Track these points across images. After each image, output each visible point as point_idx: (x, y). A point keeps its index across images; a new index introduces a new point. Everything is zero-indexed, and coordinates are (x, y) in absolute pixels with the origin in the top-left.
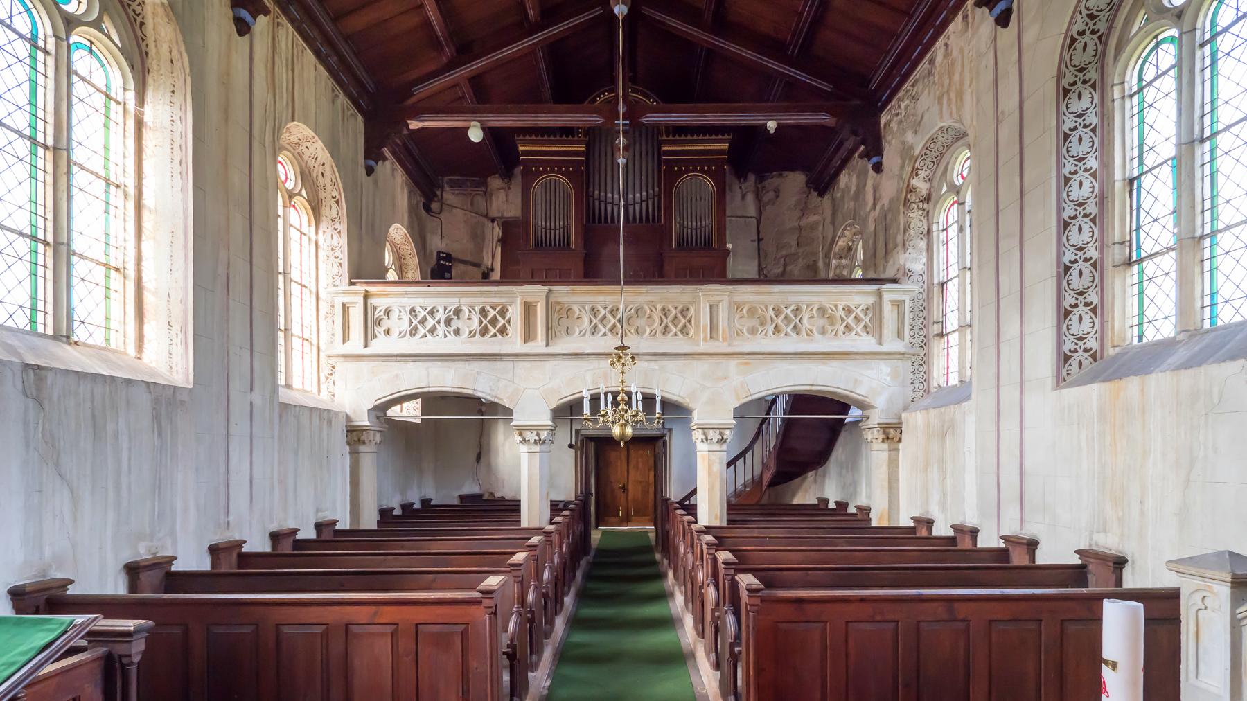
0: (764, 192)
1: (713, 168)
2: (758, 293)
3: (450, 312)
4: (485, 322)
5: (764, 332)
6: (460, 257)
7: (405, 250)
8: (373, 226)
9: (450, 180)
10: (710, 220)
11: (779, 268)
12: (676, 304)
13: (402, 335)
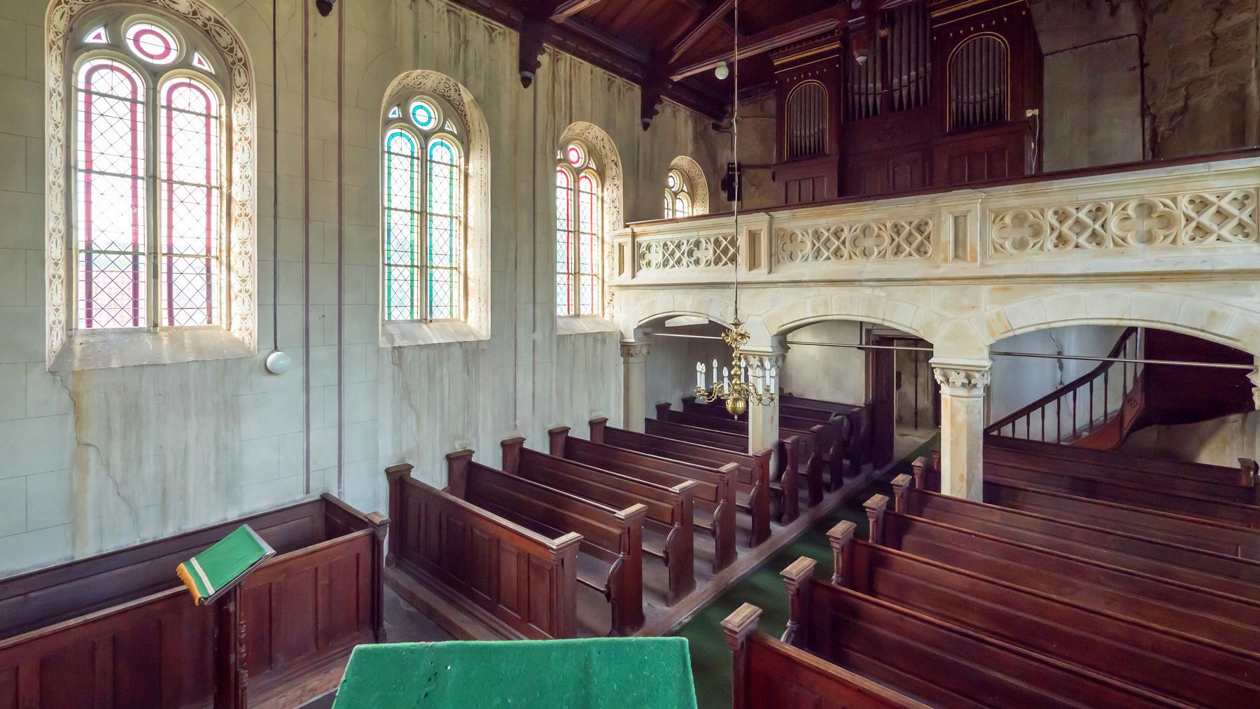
1: (1005, 19)
2: (1026, 195)
4: (718, 251)
11: (1177, 102)
12: (910, 220)
13: (658, 266)
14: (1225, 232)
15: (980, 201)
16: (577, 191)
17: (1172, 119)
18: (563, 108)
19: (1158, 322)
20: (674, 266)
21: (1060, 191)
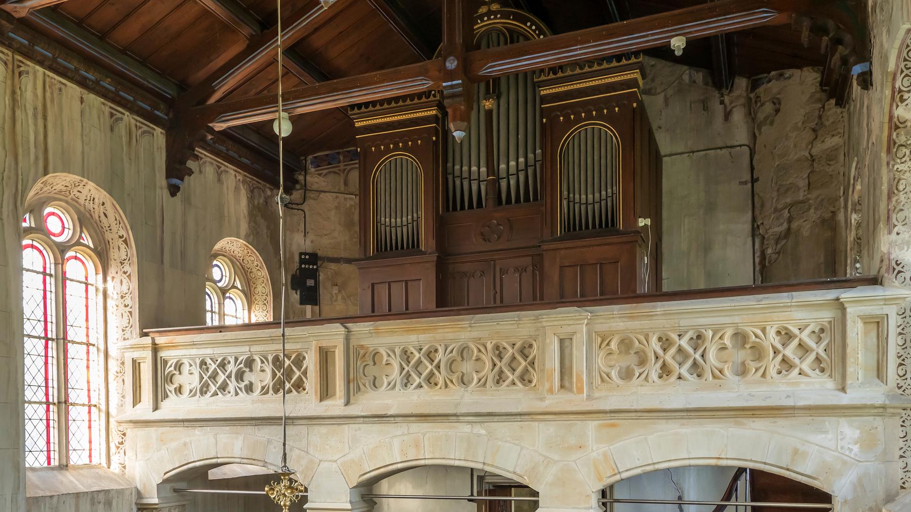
0: (759, 104)
2: (632, 318)
3: (241, 363)
5: (644, 376)
6: (330, 254)
7: (250, 262)
8: (183, 254)
9: (315, 157)
10: (614, 188)
11: (782, 224)
12: (513, 340)
13: (192, 393)
14: (805, 366)
15: (586, 321)
16: (64, 281)
17: (777, 242)
18: (32, 150)
19: (751, 461)
20: (216, 394)
21: (663, 314)
